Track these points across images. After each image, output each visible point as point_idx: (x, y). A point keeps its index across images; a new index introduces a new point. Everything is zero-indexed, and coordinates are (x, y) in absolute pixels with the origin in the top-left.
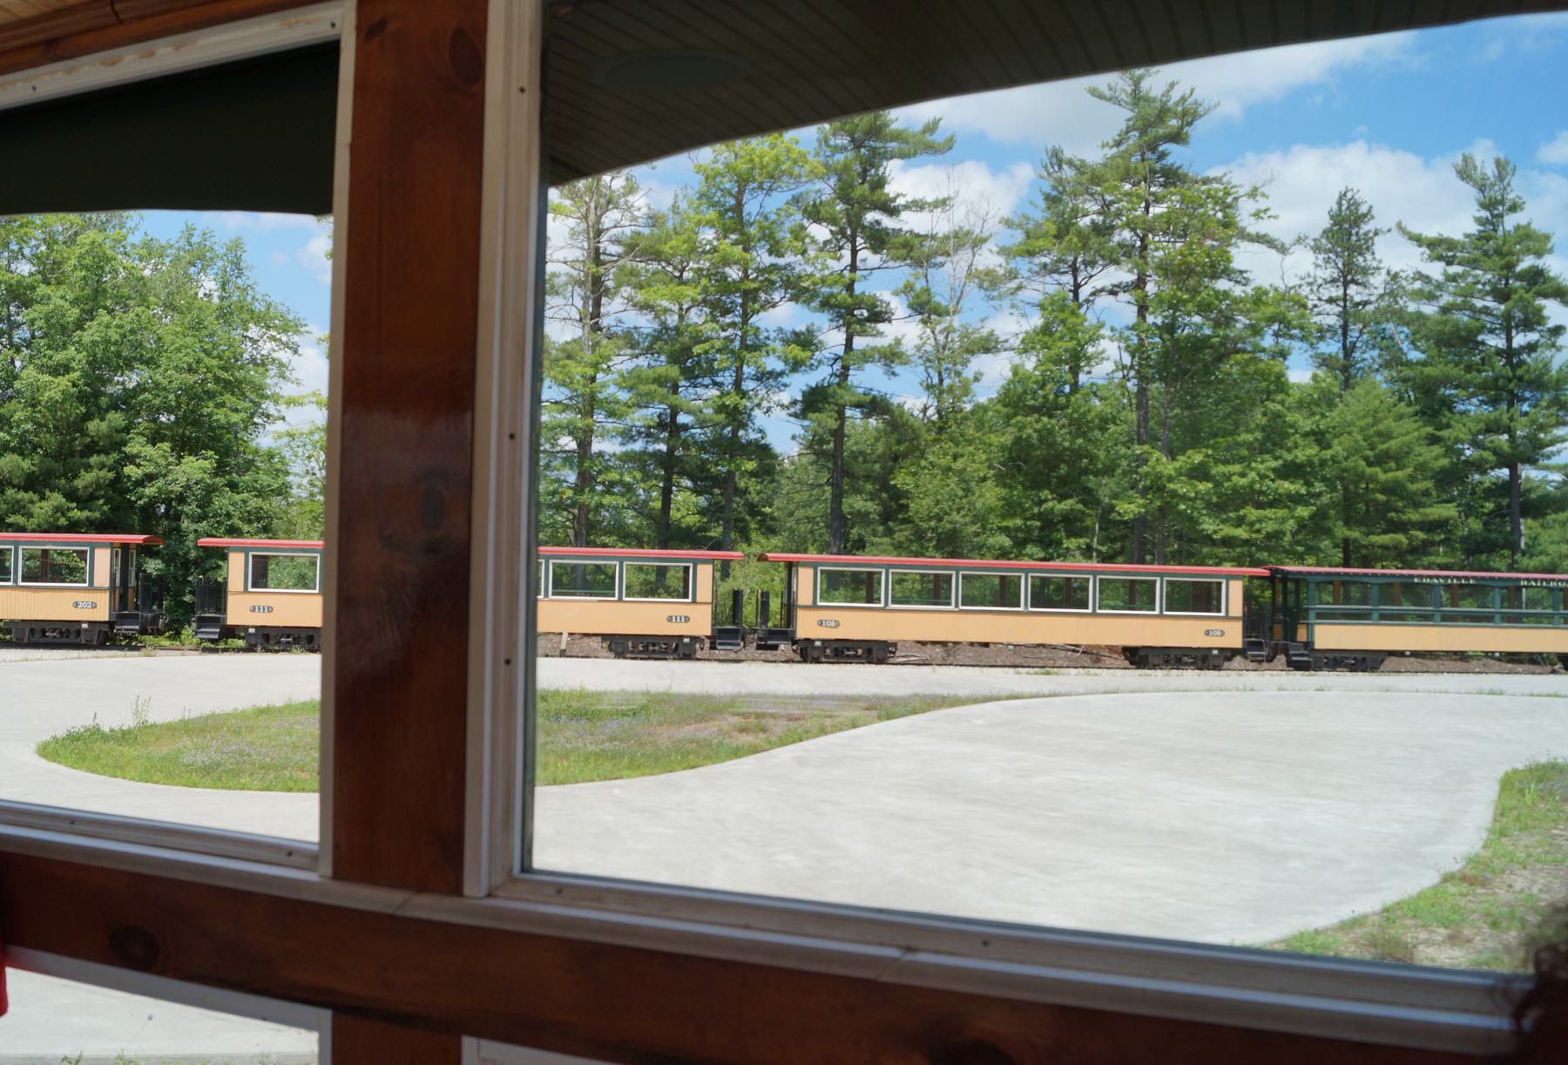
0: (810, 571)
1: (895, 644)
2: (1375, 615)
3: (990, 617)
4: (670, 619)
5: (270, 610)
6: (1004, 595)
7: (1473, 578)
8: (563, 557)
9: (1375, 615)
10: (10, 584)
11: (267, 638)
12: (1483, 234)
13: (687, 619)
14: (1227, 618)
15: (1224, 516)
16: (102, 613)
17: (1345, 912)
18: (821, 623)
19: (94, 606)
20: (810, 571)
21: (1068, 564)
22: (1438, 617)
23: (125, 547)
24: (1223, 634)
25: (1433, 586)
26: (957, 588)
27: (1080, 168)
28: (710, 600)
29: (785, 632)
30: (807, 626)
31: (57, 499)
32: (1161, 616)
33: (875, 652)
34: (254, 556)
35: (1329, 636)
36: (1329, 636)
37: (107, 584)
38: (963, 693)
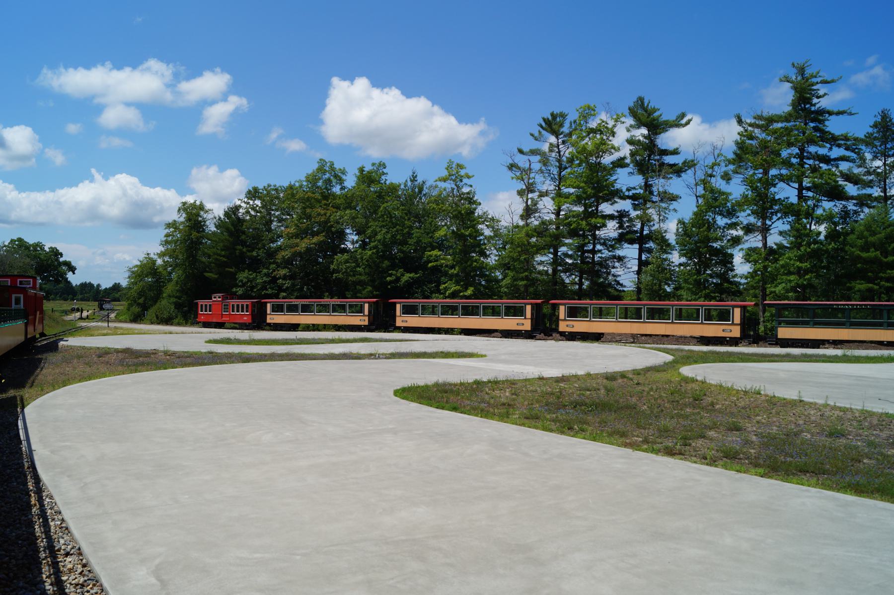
0: (563, 307)
1: (603, 334)
2: (812, 323)
3: (664, 325)
4: (518, 324)
5: (407, 321)
6: (637, 315)
7: (869, 305)
8: (485, 303)
9: (812, 323)
10: (615, 320)
11: (320, 328)
12: (170, 239)
13: (523, 324)
14: (733, 324)
15: (170, 289)
16: (366, 323)
17: (694, 465)
18: (567, 326)
19: (365, 320)
20: (563, 307)
21: (682, 302)
22: (848, 324)
23: (537, 304)
24: (731, 331)
25: (846, 309)
26: (644, 312)
27: (784, 182)
28: (739, 323)
29: (556, 330)
30: (563, 327)
31: (369, 288)
32: (702, 323)
33: (294, 327)
34: (505, 306)
35: (784, 332)
36: (784, 332)
37: (530, 317)
38: (187, 332)
